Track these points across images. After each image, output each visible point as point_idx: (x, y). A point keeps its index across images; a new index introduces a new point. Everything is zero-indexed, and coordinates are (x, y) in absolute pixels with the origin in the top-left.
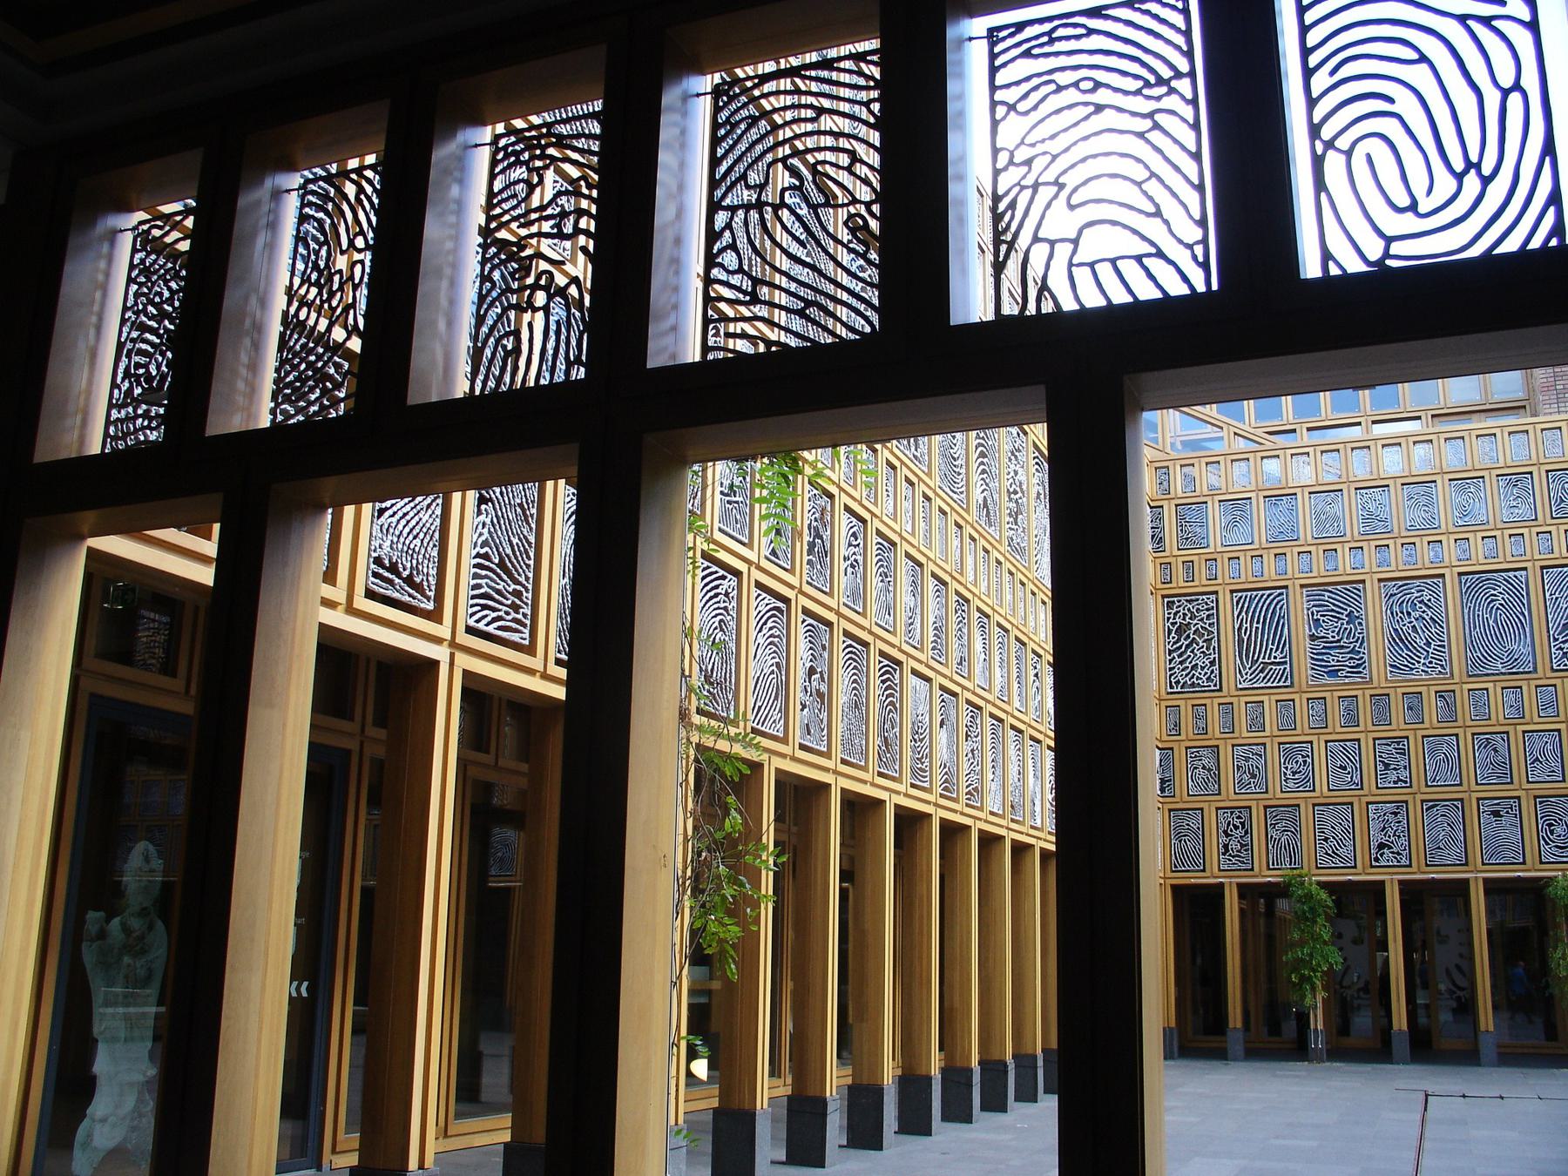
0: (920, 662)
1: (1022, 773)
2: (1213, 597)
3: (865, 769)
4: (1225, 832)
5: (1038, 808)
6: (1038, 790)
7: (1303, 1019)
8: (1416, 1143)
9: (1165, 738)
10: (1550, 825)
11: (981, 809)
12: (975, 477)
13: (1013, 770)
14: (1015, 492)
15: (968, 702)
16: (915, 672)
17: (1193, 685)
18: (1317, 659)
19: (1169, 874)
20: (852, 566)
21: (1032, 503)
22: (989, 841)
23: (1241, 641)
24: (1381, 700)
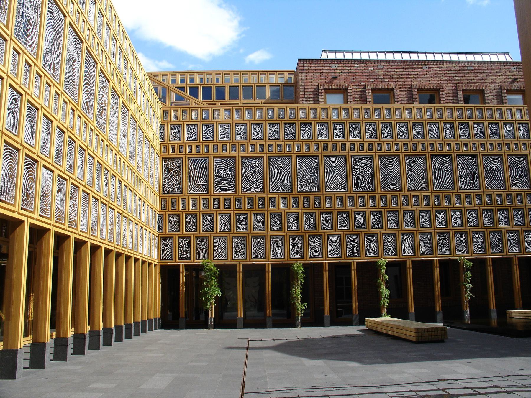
0: (61, 171)
1: (97, 216)
2: (181, 159)
3: (14, 205)
4: (181, 246)
5: (104, 231)
6: (104, 224)
7: (207, 313)
8: (244, 361)
9: (161, 210)
10: (294, 245)
11: (76, 229)
12: (82, 92)
13: (93, 216)
14: (102, 103)
15: (72, 184)
16: (44, 166)
17: (172, 191)
18: (218, 183)
19: (160, 261)
20: (13, 113)
21: (109, 110)
22: (79, 244)
23: (190, 176)
24: (239, 199)
